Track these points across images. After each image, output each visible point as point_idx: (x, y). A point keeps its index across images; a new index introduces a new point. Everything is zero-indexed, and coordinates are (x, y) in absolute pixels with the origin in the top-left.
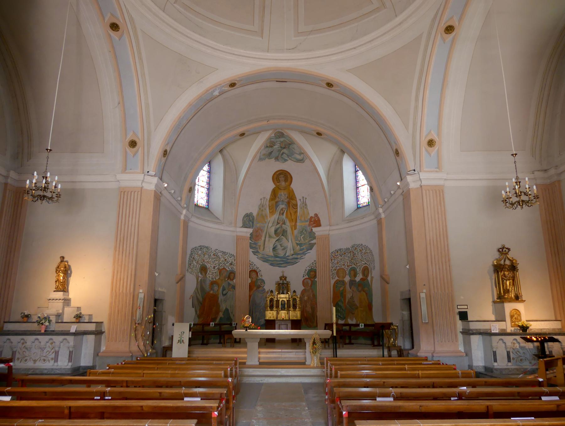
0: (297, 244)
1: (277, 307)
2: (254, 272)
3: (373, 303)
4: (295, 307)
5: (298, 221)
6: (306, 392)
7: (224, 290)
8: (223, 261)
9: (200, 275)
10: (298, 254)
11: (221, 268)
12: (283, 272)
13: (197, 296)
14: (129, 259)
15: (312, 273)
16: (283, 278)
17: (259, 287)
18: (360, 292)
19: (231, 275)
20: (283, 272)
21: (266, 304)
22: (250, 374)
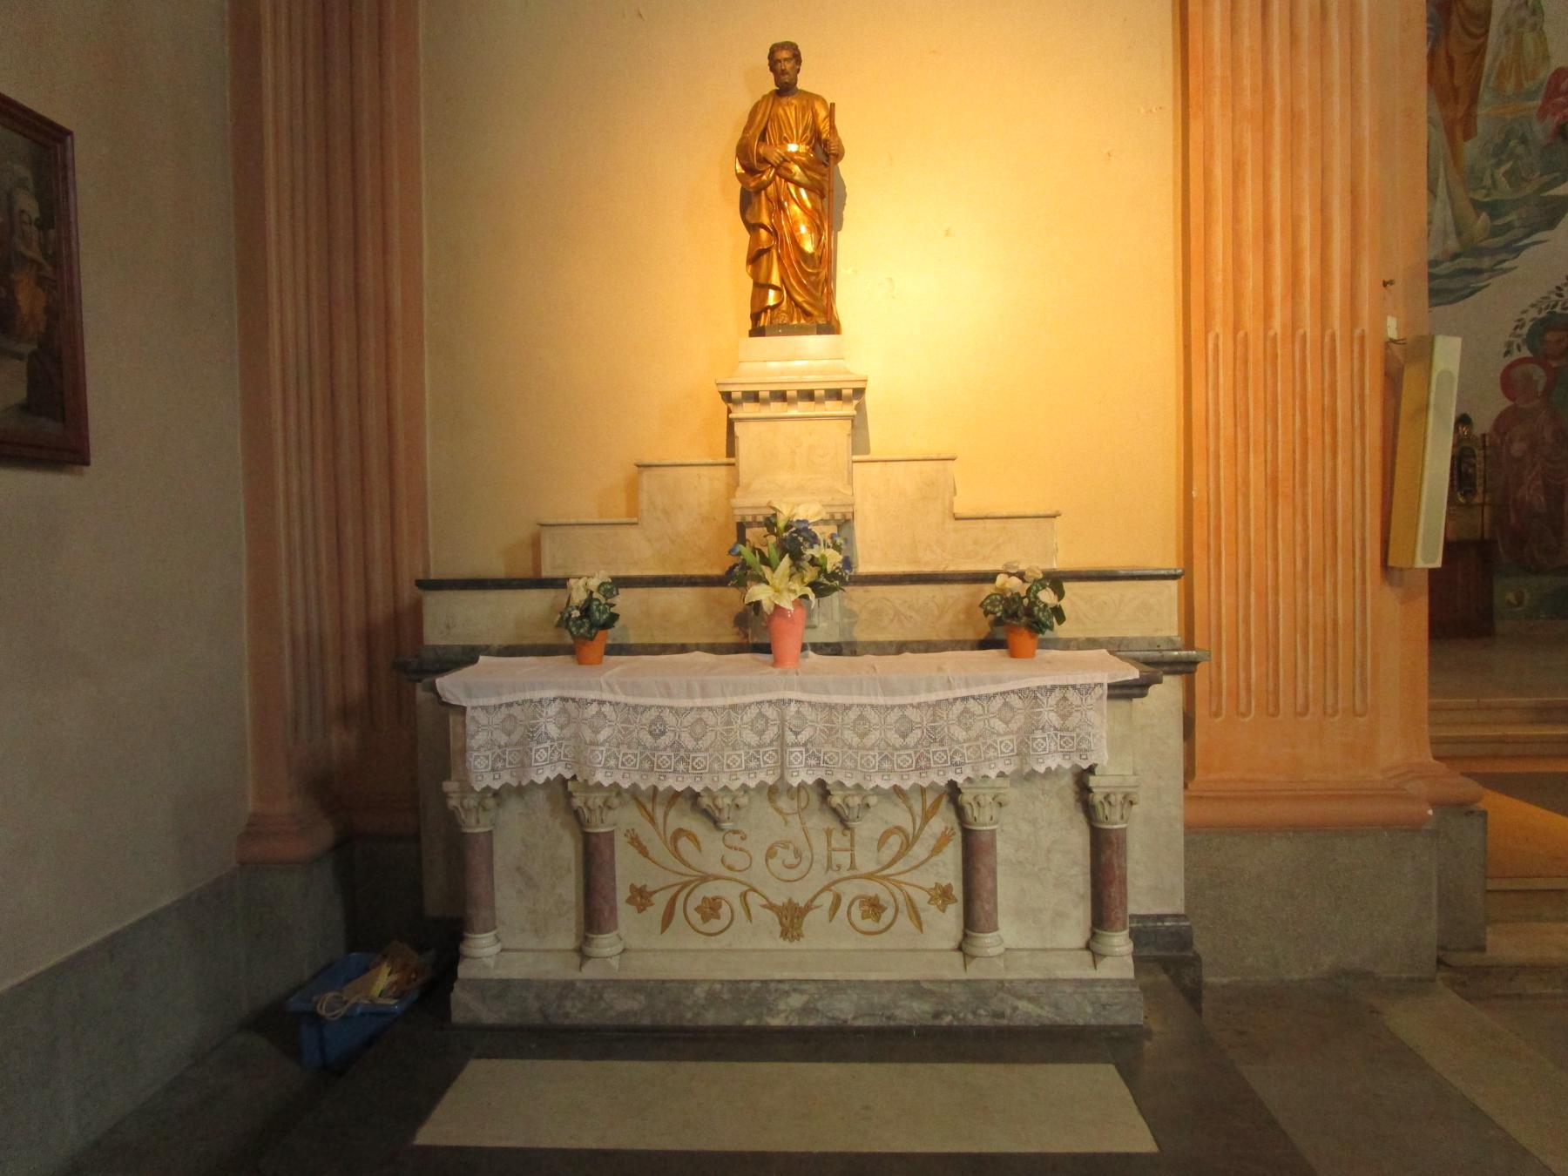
0: (1478, 206)
5: (1485, 96)
10: (1478, 252)
14: (1322, 51)
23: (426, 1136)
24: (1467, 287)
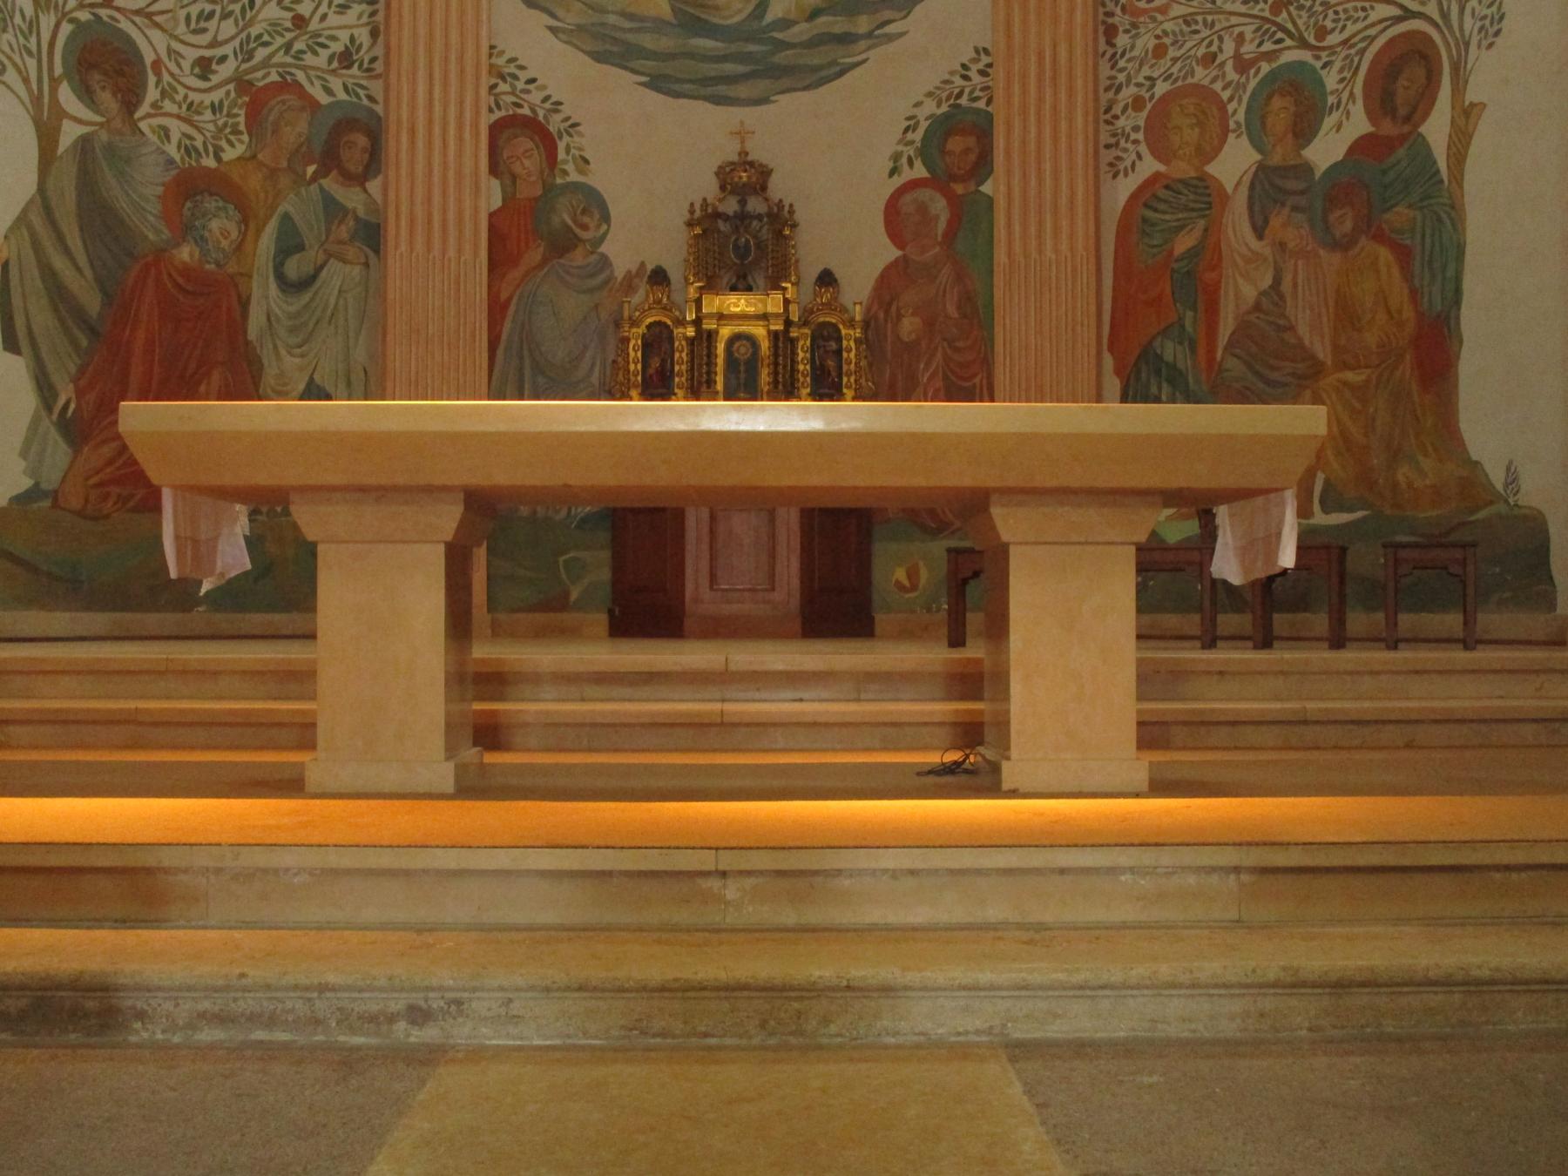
2: (522, 134)
3: (1472, 319)
7: (289, 244)
8: (275, 27)
9: (67, 97)
11: (261, 79)
12: (742, 134)
13: (48, 273)
15: (956, 144)
16: (745, 177)
17: (563, 244)
18: (1343, 245)
19: (353, 143)
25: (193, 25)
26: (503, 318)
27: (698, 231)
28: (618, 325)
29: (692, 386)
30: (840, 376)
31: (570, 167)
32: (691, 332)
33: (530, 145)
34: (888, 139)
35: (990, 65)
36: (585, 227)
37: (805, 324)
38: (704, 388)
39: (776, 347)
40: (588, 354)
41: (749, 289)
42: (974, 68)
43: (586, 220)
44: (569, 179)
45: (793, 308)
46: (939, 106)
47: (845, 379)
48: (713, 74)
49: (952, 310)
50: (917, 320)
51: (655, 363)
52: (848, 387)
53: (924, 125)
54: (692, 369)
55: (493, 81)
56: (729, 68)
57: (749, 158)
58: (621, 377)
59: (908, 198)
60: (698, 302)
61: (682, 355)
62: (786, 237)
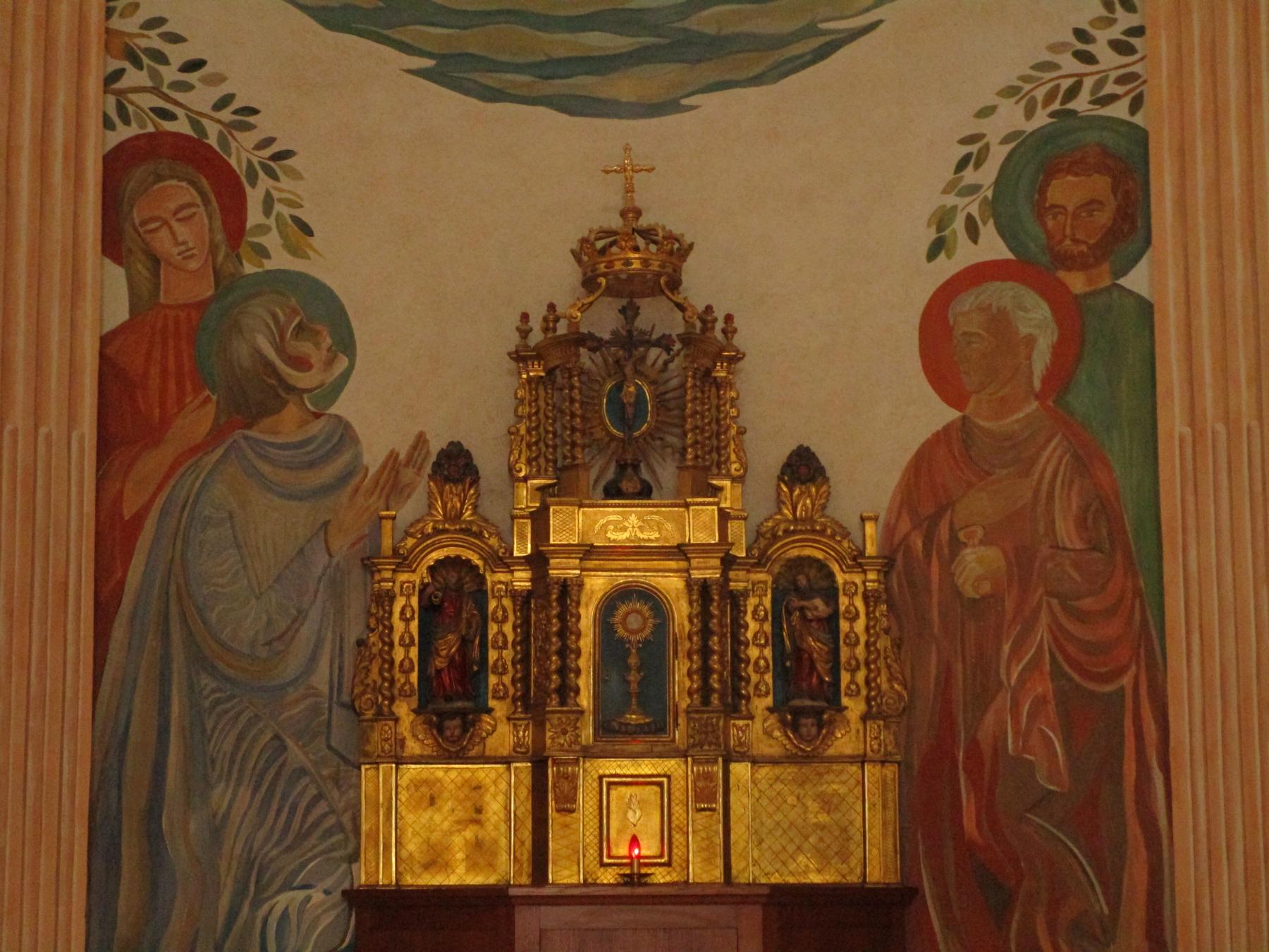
1: (540, 697)
4: (807, 698)
6: (810, 566)
15: (1067, 191)
16: (633, 265)
20: (627, 173)
21: (371, 649)
22: (585, 909)
23: (1009, 255)
24: (811, 30)
25: (559, 464)
26: (128, 555)
27: (537, 371)
28: (369, 565)
29: (525, 697)
30: (835, 672)
31: (271, 241)
32: (522, 579)
33: (191, 195)
34: (924, 187)
35: (1138, 31)
36: (301, 363)
37: (759, 561)
38: (553, 703)
39: (705, 615)
40: (307, 631)
41: (645, 492)
42: (1103, 36)
43: (304, 347)
44: (269, 265)
45: (735, 528)
46: (1030, 113)
47: (845, 677)
48: (561, 53)
49: (1066, 531)
50: (993, 554)
51: (448, 645)
52: (854, 694)
53: (999, 154)
54: (524, 660)
55: (115, 64)
56: (598, 41)
57: (644, 222)
58: (374, 674)
59: (967, 302)
60: (540, 520)
61: (503, 630)
62: (718, 385)
